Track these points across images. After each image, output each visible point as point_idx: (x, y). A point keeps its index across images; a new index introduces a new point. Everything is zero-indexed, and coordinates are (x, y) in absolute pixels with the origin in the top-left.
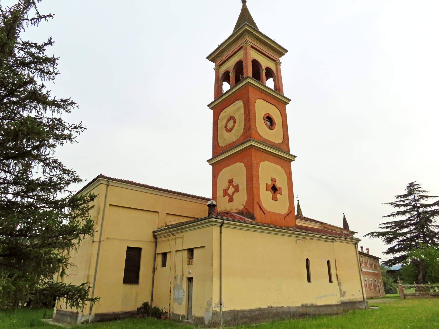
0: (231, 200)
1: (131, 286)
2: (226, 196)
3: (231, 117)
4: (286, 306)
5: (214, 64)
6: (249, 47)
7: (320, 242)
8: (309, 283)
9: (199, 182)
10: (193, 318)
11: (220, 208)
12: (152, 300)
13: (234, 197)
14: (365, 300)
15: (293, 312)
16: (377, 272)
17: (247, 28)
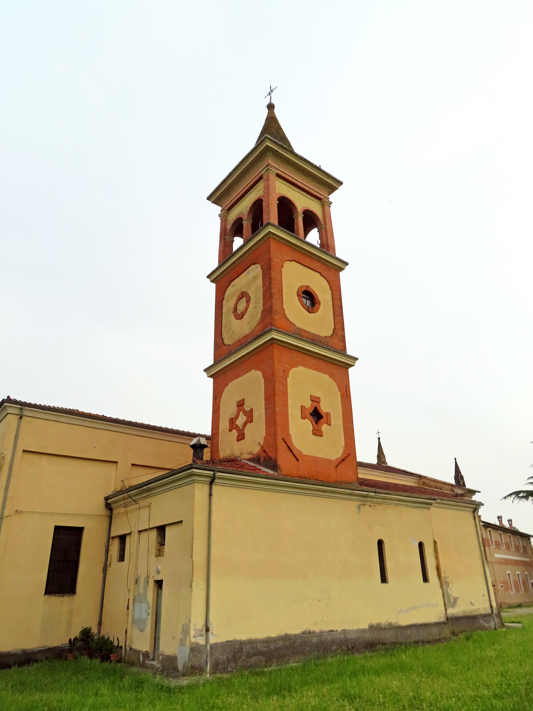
0: (241, 437)
1: (61, 599)
2: (234, 431)
3: (242, 293)
4: (339, 630)
5: (220, 208)
6: (272, 177)
7: (403, 509)
8: (384, 585)
9: (188, 406)
10: (161, 658)
11: (223, 454)
12: (100, 624)
13: (246, 431)
14: (495, 611)
15: (352, 639)
16: (528, 560)
17: (268, 143)
